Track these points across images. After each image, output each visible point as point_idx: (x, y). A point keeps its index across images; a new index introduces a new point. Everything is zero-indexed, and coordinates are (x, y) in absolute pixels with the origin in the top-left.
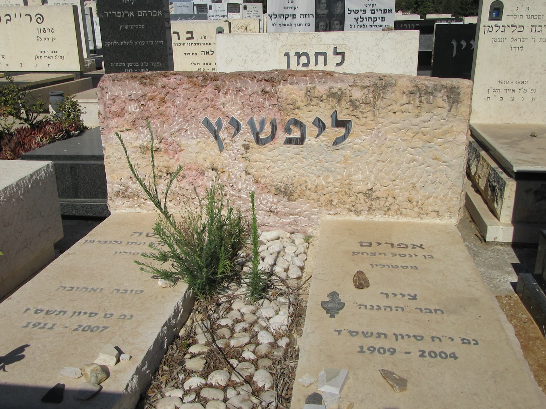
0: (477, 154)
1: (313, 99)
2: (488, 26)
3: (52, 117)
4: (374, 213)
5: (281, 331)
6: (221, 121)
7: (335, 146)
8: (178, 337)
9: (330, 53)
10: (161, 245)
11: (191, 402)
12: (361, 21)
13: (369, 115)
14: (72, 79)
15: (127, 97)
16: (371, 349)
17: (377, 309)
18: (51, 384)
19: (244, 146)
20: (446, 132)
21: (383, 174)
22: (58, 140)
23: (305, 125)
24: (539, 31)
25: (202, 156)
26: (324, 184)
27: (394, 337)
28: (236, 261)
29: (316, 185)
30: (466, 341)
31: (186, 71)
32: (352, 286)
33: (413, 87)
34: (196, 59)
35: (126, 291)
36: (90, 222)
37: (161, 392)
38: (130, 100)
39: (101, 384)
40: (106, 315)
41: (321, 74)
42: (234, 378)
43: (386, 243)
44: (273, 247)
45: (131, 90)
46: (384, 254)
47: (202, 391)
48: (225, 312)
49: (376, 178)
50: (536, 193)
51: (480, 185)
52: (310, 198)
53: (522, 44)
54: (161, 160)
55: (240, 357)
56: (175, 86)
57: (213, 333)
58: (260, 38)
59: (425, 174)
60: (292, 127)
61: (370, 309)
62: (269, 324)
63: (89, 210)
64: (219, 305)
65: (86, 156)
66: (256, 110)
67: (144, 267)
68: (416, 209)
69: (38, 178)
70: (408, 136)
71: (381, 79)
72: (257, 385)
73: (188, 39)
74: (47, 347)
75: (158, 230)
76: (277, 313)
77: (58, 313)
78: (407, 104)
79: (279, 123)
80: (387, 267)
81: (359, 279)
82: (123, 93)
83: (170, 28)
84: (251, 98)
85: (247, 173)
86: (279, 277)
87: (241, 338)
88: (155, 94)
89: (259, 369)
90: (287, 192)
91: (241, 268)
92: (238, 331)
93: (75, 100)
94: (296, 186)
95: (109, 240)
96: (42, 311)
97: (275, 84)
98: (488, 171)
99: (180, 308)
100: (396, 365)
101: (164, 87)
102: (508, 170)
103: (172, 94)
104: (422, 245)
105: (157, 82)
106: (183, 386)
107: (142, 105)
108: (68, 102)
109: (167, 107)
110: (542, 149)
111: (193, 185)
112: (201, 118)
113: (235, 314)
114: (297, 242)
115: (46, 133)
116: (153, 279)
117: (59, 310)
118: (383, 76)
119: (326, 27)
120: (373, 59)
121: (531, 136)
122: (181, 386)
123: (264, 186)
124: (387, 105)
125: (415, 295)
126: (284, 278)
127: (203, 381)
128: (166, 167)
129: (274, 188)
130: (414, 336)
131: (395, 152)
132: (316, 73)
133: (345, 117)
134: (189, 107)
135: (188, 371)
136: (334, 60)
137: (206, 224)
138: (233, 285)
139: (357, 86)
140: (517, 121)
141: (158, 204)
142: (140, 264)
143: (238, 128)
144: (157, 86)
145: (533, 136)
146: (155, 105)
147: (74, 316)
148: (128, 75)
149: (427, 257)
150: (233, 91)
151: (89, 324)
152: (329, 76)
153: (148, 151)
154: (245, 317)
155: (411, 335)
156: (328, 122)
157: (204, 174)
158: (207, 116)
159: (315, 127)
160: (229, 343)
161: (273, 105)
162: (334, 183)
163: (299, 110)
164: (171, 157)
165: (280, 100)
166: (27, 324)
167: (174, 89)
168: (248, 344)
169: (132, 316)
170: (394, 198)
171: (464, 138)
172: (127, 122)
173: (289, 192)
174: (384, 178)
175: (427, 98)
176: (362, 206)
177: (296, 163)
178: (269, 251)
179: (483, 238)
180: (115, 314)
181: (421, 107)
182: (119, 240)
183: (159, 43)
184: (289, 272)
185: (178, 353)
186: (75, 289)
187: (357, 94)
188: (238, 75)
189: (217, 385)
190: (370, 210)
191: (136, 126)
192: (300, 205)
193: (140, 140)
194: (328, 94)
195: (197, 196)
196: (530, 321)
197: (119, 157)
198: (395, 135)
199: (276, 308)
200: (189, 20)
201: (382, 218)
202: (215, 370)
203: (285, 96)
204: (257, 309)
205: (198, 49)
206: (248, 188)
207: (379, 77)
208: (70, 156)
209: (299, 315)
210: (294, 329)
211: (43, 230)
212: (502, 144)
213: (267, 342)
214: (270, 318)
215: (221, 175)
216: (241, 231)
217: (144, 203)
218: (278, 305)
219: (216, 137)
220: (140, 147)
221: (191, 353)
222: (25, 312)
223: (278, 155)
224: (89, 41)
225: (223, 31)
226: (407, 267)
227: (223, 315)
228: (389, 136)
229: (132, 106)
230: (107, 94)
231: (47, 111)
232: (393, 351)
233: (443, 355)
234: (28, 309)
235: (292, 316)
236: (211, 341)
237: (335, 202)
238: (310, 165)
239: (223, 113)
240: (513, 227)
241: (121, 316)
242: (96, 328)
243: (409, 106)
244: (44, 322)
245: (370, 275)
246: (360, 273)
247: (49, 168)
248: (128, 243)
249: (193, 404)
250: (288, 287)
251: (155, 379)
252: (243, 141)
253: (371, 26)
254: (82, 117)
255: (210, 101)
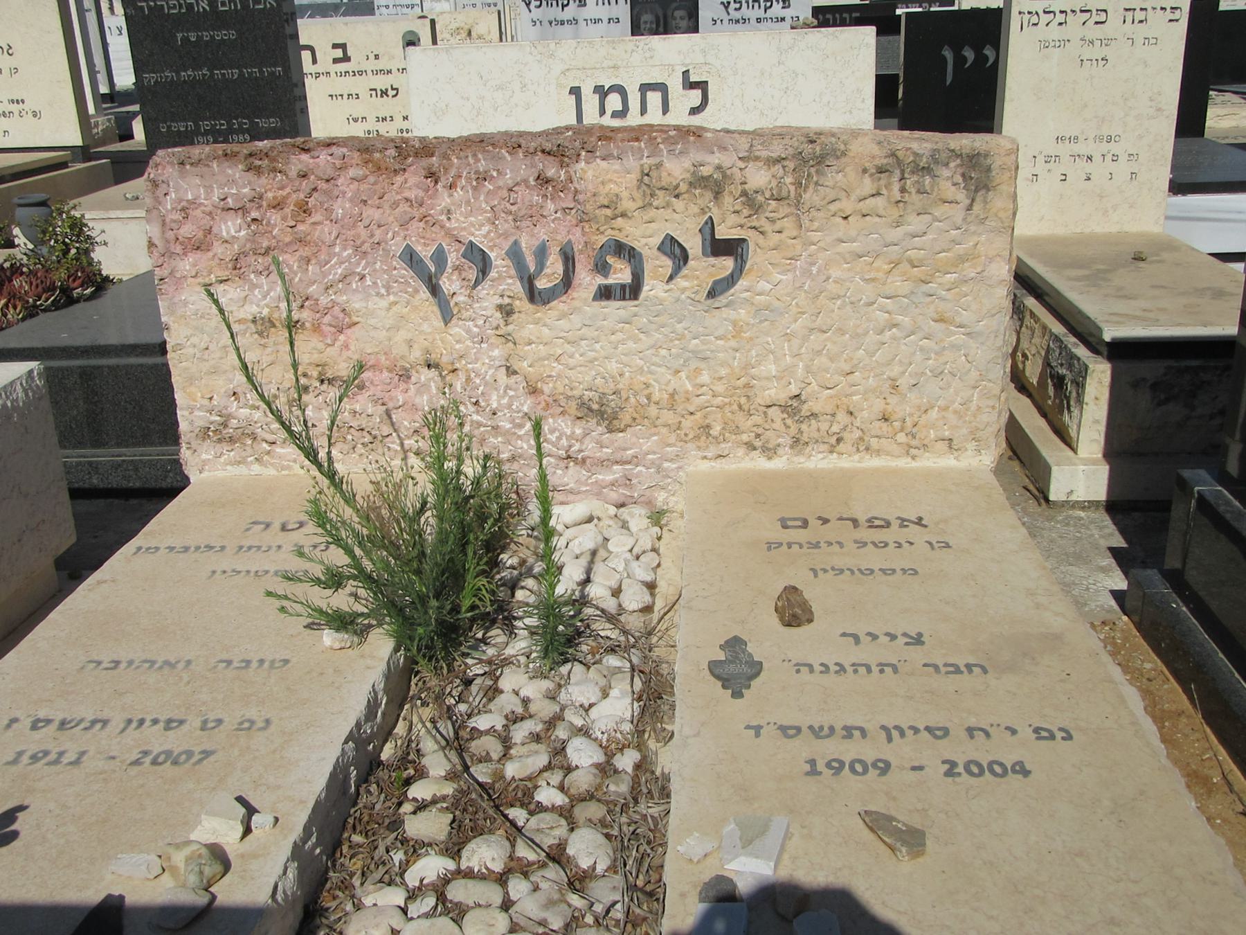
0: (1017, 304)
1: (657, 192)
2: (1029, 13)
3: (25, 258)
4: (807, 451)
5: (619, 735)
6: (443, 251)
7: (710, 301)
8: (380, 763)
9: (675, 84)
10: (318, 549)
11: (427, 915)
12: (736, 9)
13: (787, 225)
14: (63, 165)
15: (216, 204)
16: (835, 764)
17: (836, 672)
18: (92, 895)
19: (500, 307)
20: (962, 259)
21: (824, 360)
22: (45, 311)
23: (640, 255)
24: (1141, 22)
25: (402, 335)
26: (691, 389)
27: (883, 734)
28: (498, 577)
29: (671, 391)
30: (1044, 734)
31: (353, 138)
32: (774, 620)
33: (886, 157)
34: (357, 109)
35: (248, 662)
36: (134, 502)
37: (353, 897)
38: (223, 209)
39: (211, 889)
40: (205, 722)
41: (672, 133)
42: (524, 852)
43: (841, 519)
44: (580, 539)
45: (226, 185)
46: (838, 543)
47: (449, 887)
48: (485, 699)
49: (808, 370)
50: (1155, 387)
51: (1027, 374)
52: (658, 422)
53: (1105, 51)
54: (309, 349)
55: (530, 803)
56: (330, 172)
57: (462, 750)
58: (509, 53)
59: (919, 356)
60: (610, 260)
61: (821, 672)
62: (589, 722)
63: (131, 473)
64: (468, 682)
65: (116, 347)
66: (524, 224)
67: (285, 603)
68: (901, 437)
69: (9, 404)
70: (878, 270)
71: (812, 142)
72: (577, 866)
73: (336, 61)
74: (70, 808)
75: (321, 518)
76: (605, 695)
77: (88, 724)
78: (873, 195)
79: (581, 252)
80: (848, 572)
81: (791, 605)
82: (207, 193)
83: (295, 36)
84: (513, 195)
85: (511, 372)
86: (603, 611)
87: (528, 756)
88: (284, 193)
89: (577, 827)
90: (605, 412)
91: (509, 592)
92: (518, 741)
93: (77, 214)
94: (624, 396)
95: (193, 544)
96: (48, 721)
97: (566, 159)
98: (1044, 342)
99: (380, 695)
100: (894, 799)
101: (304, 176)
102: (1091, 339)
103: (325, 192)
104: (920, 519)
105: (288, 163)
106: (403, 879)
107: (254, 220)
108: (63, 221)
109: (314, 223)
110: (1163, 287)
111: (383, 404)
112: (397, 246)
113: (507, 702)
114: (634, 526)
115: (14, 296)
116: (309, 631)
117: (91, 718)
118: (816, 133)
119: (658, 25)
120: (773, 97)
121: (1135, 259)
122: (398, 879)
123: (550, 400)
124: (828, 199)
125: (920, 635)
126: (613, 611)
127: (451, 865)
128: (318, 366)
129: (573, 405)
130: (927, 729)
131: (848, 308)
132: (661, 131)
133: (733, 231)
134: (366, 222)
135: (411, 843)
136: (681, 101)
137: (428, 495)
138: (497, 635)
139: (757, 159)
140: (1100, 226)
141: (311, 454)
142: (279, 597)
143: (484, 266)
144: (287, 177)
145: (1139, 258)
146: (284, 219)
147: (128, 731)
148: (215, 151)
149: (936, 545)
150: (469, 179)
151: (166, 747)
152: (692, 138)
153: (273, 329)
154: (533, 708)
155: (921, 727)
156: (694, 244)
157: (409, 377)
158: (410, 240)
159: (664, 258)
160: (502, 770)
161: (564, 209)
162: (712, 387)
163: (626, 220)
164: (329, 341)
165: (580, 197)
166: (15, 756)
167: (328, 181)
168: (547, 770)
169: (268, 722)
170: (851, 413)
171: (1003, 272)
172: (218, 261)
173: (609, 411)
174: (827, 370)
175: (917, 182)
176: (779, 437)
177: (623, 342)
178: (572, 551)
179: (1042, 495)
180: (227, 720)
181: (905, 202)
182: (217, 544)
183: (273, 73)
184: (622, 595)
185: (384, 802)
186: (123, 665)
187: (758, 178)
188: (479, 142)
189: (484, 871)
190: (797, 443)
191: (242, 270)
192: (636, 441)
193: (252, 303)
194: (692, 180)
195: (395, 431)
196: (1162, 677)
197: (203, 345)
198: (849, 270)
199: (603, 682)
200: (332, 16)
201: (826, 461)
202: (475, 837)
203: (590, 187)
204: (560, 686)
205: (360, 85)
206: (514, 407)
207: (807, 136)
208: (77, 348)
209: (656, 694)
210: (648, 729)
211: (27, 526)
212: (1078, 279)
213: (591, 762)
214: (591, 706)
215: (448, 378)
216: (503, 508)
217: (268, 453)
218: (606, 673)
219: (435, 290)
220: (254, 321)
221: (415, 799)
222: (9, 726)
223: (580, 325)
224: (99, 72)
225: (419, 40)
226: (894, 571)
227: (481, 706)
228: (835, 273)
229: (229, 223)
230: (168, 197)
231: (10, 244)
232: (884, 767)
233: (998, 770)
234: (14, 720)
235: (639, 699)
236: (459, 768)
237: (716, 430)
238: (656, 347)
239: (448, 233)
240: (1107, 467)
241: (241, 723)
242: (184, 757)
243: (879, 202)
244: (57, 750)
245: (813, 593)
246: (792, 590)
247: (33, 378)
248: (241, 547)
249: (434, 920)
250: (625, 632)
251: (334, 866)
252: (497, 297)
253: (759, 20)
254: (98, 254)
255: (415, 205)
